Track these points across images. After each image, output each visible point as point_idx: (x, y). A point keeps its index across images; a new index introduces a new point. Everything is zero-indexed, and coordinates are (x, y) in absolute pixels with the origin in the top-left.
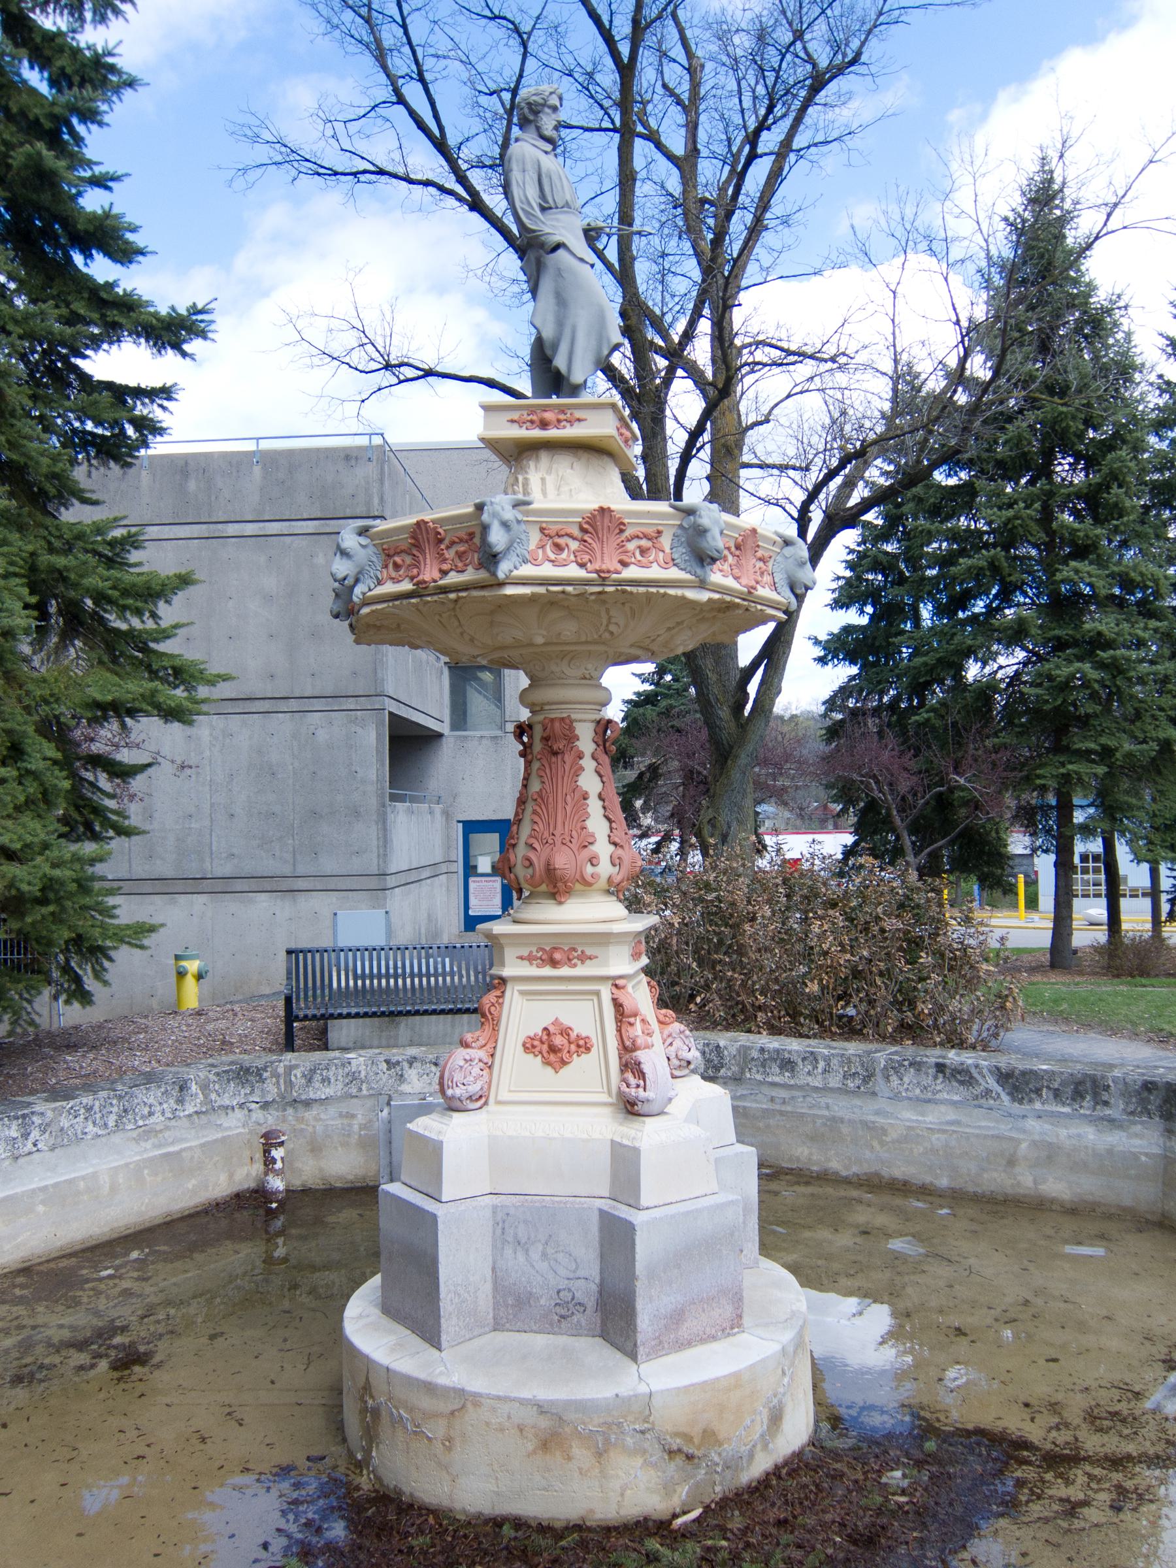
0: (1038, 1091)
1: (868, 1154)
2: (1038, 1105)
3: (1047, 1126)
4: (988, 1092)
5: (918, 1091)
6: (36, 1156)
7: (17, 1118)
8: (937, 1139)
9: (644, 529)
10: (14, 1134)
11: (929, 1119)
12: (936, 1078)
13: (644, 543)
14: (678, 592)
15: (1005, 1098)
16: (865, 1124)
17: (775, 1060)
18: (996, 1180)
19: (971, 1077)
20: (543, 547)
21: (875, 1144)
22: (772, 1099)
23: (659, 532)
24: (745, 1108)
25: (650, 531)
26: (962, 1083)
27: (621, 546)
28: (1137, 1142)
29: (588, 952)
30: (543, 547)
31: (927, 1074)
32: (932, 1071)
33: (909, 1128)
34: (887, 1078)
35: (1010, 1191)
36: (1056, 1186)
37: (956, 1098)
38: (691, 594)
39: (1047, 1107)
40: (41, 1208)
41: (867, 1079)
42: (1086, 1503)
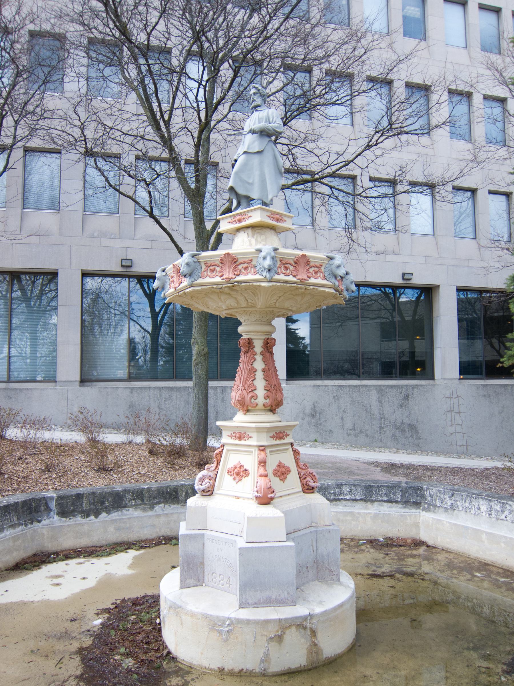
6: (505, 522)
7: (500, 503)
9: (244, 260)
10: (499, 509)
13: (316, 269)
14: (258, 284)
23: (321, 266)
25: (318, 264)
27: (308, 270)
38: (263, 284)
40: (503, 545)
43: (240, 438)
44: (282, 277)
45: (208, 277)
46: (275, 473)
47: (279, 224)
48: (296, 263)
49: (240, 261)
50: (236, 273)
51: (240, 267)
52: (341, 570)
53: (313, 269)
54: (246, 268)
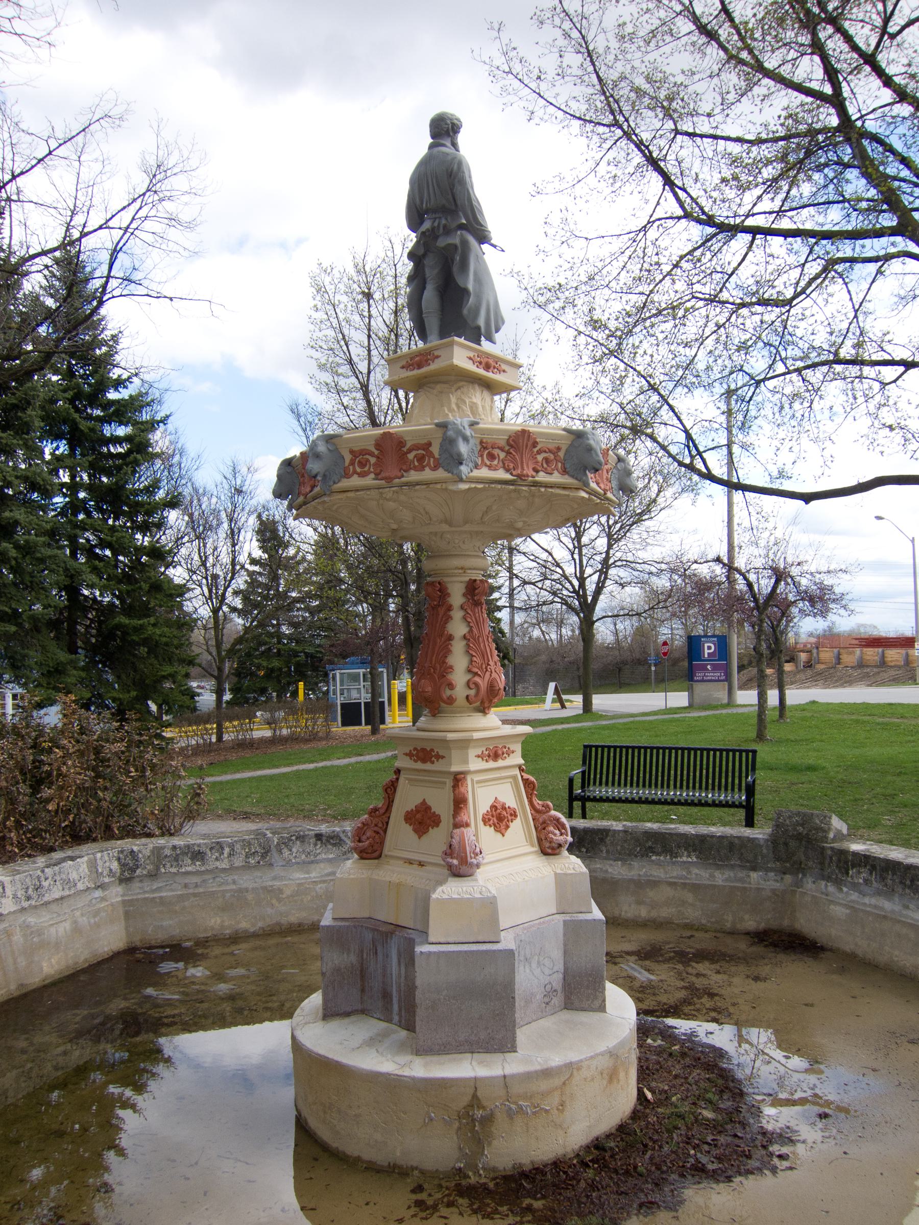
1: (269, 911)
5: (303, 857)
11: (313, 875)
12: (316, 845)
16: (265, 888)
17: (187, 854)
19: (341, 840)
21: (274, 901)
22: (186, 886)
24: (161, 898)
26: (334, 845)
32: (313, 840)
33: (300, 885)
34: (280, 852)
37: (331, 856)
41: (266, 853)
43: (424, 761)
44: (484, 473)
46: (435, 821)
47: (490, 375)
52: (609, 986)
53: (544, 455)
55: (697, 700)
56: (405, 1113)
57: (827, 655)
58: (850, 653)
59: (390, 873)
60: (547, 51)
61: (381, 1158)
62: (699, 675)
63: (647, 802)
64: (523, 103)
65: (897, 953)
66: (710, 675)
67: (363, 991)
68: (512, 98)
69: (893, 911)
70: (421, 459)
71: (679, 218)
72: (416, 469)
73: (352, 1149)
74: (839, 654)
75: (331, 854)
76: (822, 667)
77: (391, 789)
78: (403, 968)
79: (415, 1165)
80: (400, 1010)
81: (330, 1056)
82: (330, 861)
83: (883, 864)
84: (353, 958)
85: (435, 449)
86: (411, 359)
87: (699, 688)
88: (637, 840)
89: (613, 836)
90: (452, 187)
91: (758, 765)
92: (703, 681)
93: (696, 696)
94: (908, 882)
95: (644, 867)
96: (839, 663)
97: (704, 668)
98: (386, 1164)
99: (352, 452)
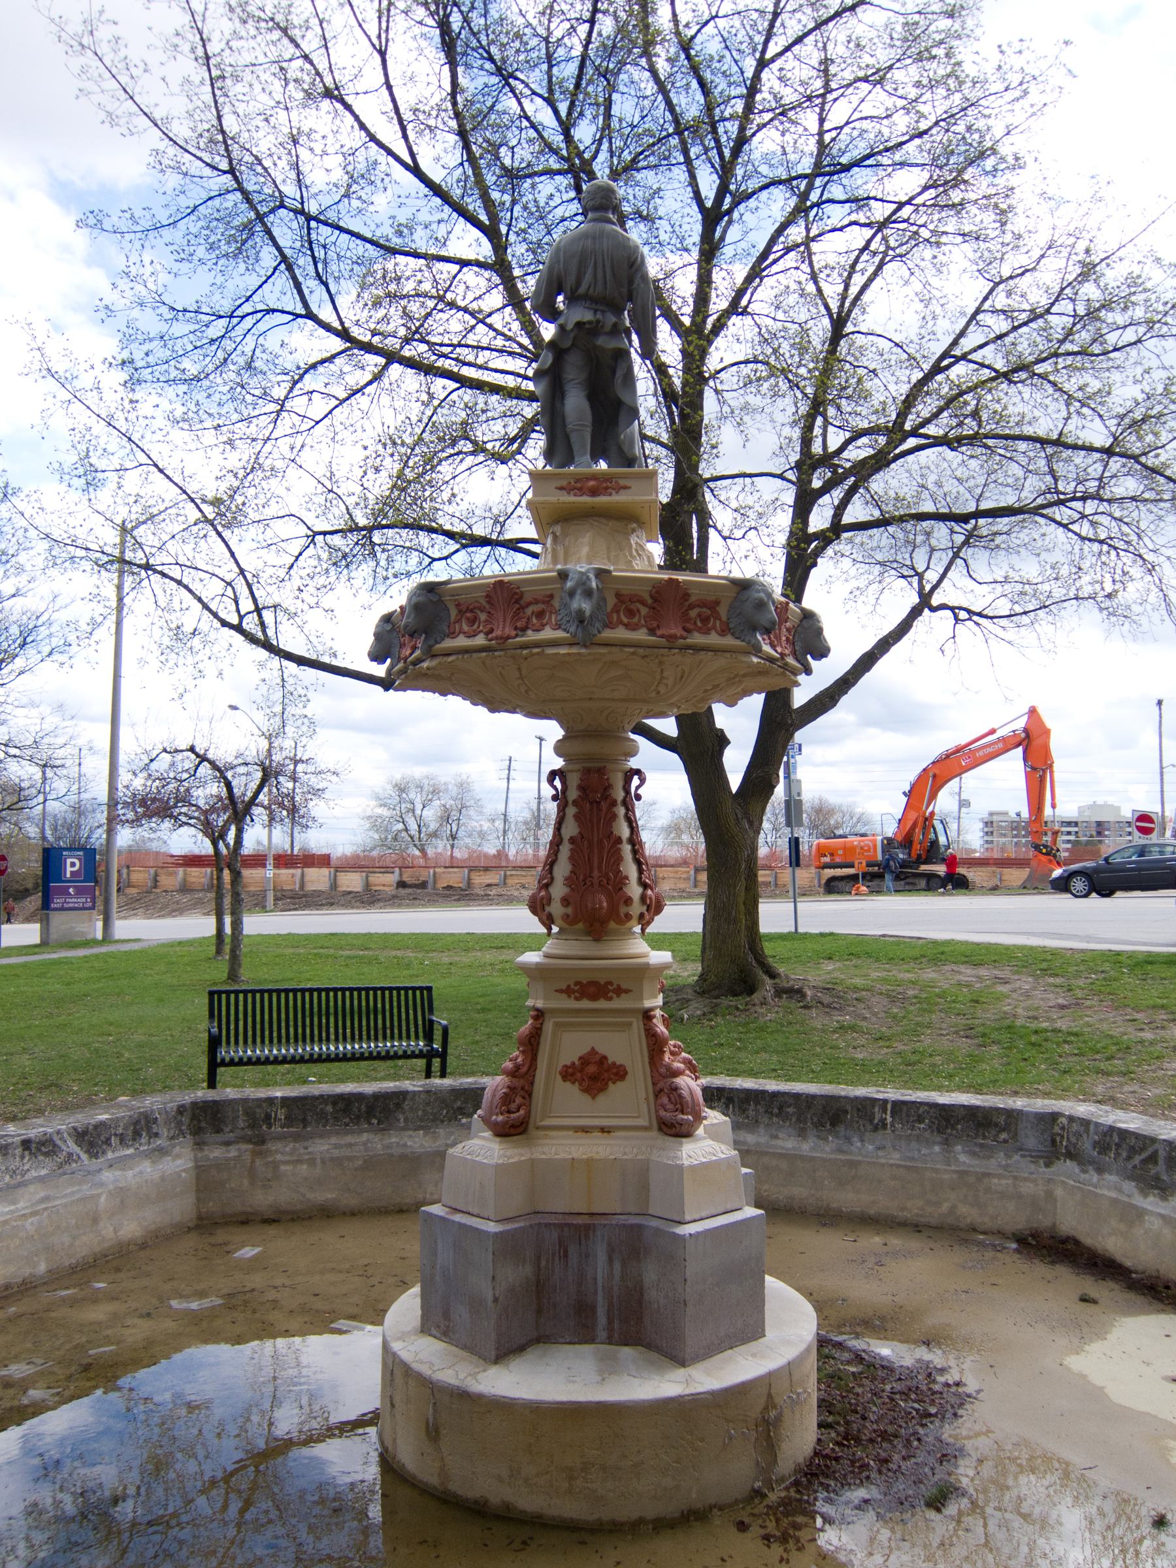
0: (107, 1142)
2: (110, 1155)
3: (118, 1173)
4: (70, 1155)
5: (7, 1178)
8: (30, 1224)
11: (21, 1205)
12: (22, 1157)
15: (84, 1156)
18: (87, 1244)
19: (55, 1145)
20: (618, 612)
26: (47, 1154)
27: (686, 614)
28: (179, 1162)
29: (624, 986)
30: (618, 612)
31: (14, 1156)
32: (18, 1151)
35: (97, 1249)
36: (131, 1228)
37: (43, 1172)
39: (117, 1154)
42: (314, 1502)
43: (594, 997)
45: (461, 637)
48: (655, 600)
49: (527, 598)
50: (519, 624)
51: (529, 611)
54: (540, 615)
55: (54, 935)
56: (702, 1440)
57: (140, 876)
58: (171, 874)
59: (558, 1148)
60: (160, 44)
61: (670, 1509)
62: (57, 902)
63: (362, 1057)
64: (104, 99)
65: (766, 1187)
66: (72, 901)
67: (539, 1312)
68: (90, 86)
69: (758, 1144)
70: (705, 620)
71: (299, 316)
72: (700, 630)
73: (629, 1513)
74: (156, 875)
75: (40, 1169)
76: (133, 891)
77: (531, 1043)
78: (617, 1266)
79: (713, 1502)
80: (610, 1321)
81: (581, 1398)
82: (41, 1179)
83: (742, 1096)
84: (528, 1270)
85: (723, 611)
86: (577, 481)
87: (59, 921)
88: (443, 1101)
89: (413, 1099)
90: (631, 282)
91: (436, 1004)
92: (63, 909)
93: (53, 930)
94: (776, 1111)
95: (451, 1134)
96: (156, 887)
97: (64, 892)
98: (677, 1515)
99: (618, 595)
